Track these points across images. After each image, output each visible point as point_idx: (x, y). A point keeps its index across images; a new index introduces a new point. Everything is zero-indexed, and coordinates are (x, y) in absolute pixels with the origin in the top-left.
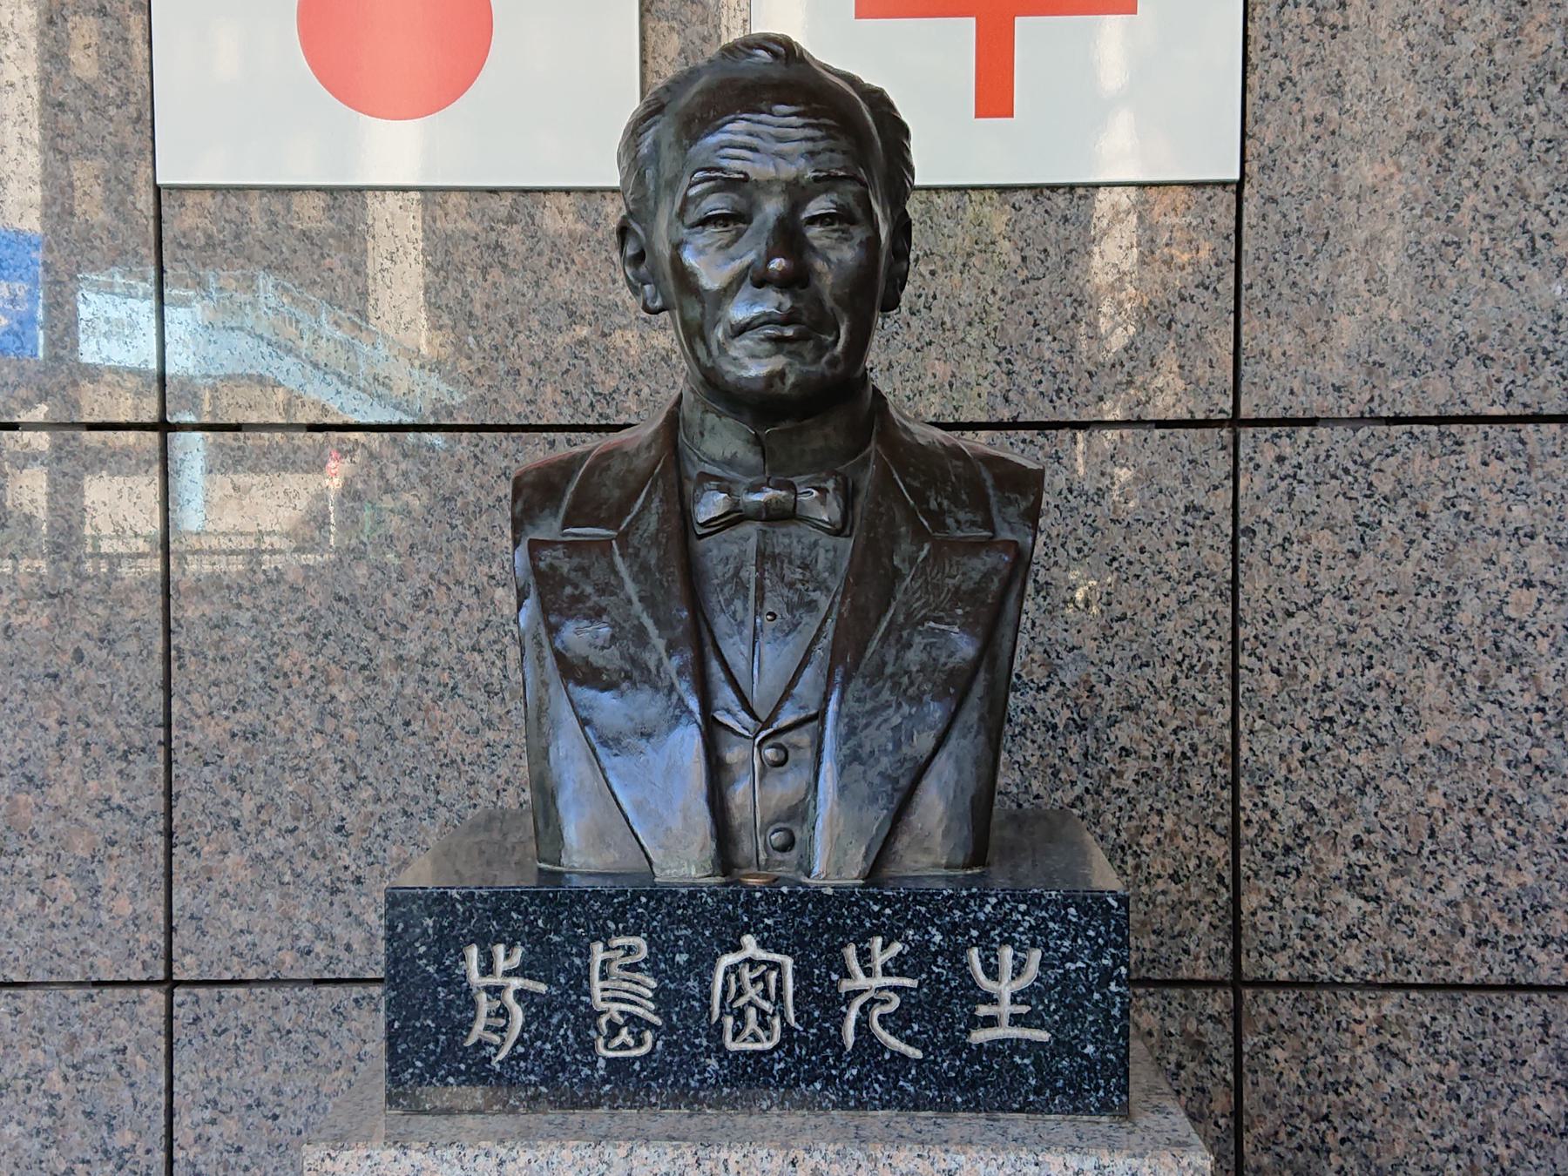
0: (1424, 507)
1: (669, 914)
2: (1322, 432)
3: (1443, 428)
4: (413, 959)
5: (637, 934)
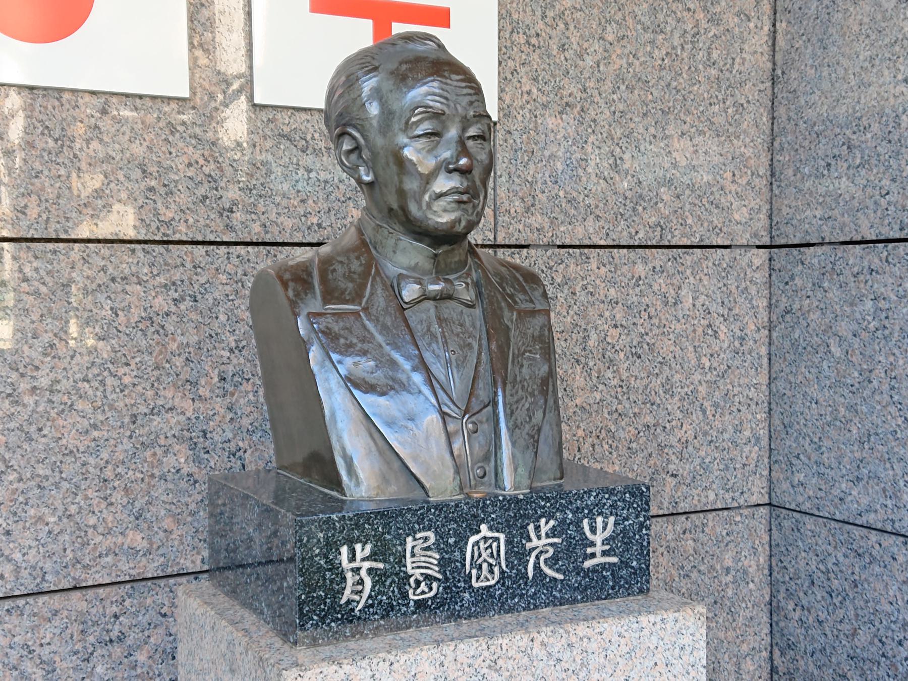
0: (575, 289)
1: (445, 517)
2: (532, 252)
3: (582, 250)
4: (312, 558)
5: (429, 530)
